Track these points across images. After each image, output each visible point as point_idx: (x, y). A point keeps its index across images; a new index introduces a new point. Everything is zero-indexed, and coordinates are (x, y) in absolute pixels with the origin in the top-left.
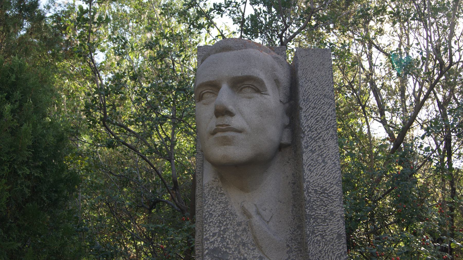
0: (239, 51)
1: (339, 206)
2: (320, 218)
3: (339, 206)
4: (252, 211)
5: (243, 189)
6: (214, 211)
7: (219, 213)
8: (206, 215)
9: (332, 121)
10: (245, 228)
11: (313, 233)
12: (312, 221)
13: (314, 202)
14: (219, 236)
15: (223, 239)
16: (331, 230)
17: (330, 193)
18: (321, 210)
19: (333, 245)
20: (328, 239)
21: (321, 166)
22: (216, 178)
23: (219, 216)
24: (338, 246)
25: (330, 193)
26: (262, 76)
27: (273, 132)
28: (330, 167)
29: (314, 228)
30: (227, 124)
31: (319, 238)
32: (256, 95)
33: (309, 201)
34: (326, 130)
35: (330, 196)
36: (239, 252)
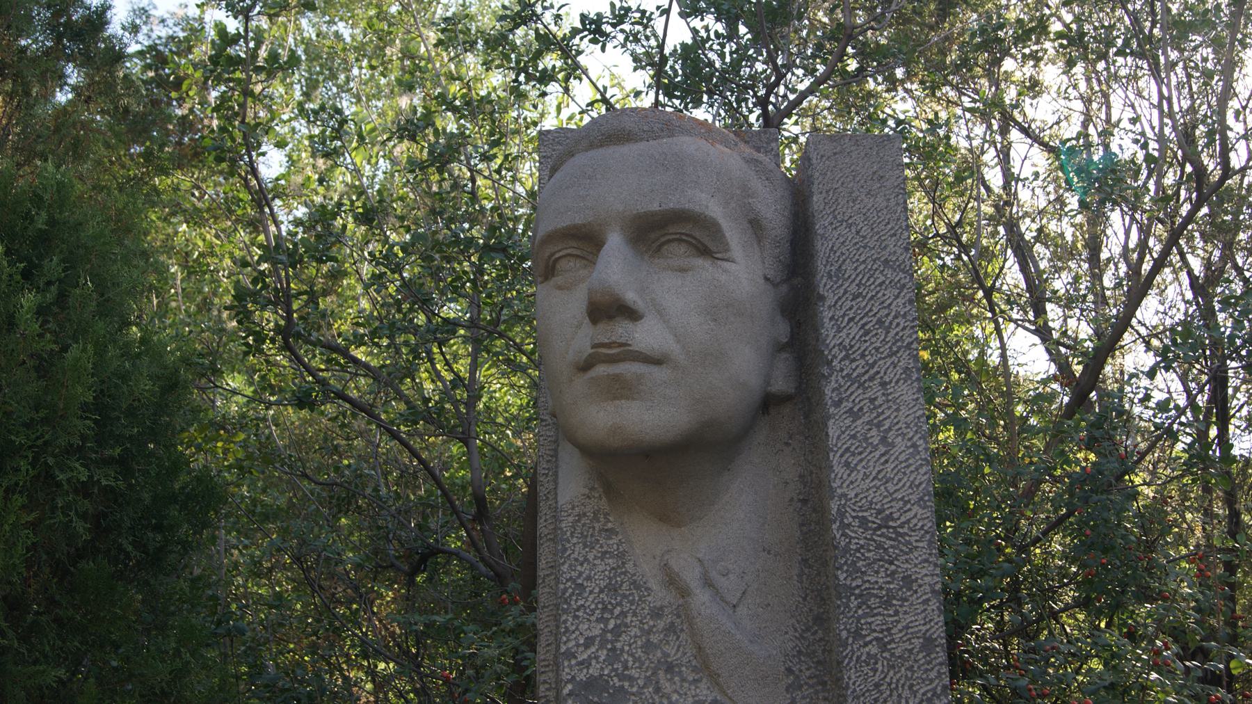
1: (926, 561)
3: (926, 561)
4: (692, 576)
5: (668, 517)
6: (589, 578)
7: (603, 584)
8: (566, 590)
9: (907, 332)
10: (672, 623)
11: (857, 634)
12: (854, 603)
13: (858, 550)
14: (601, 647)
15: (614, 655)
16: (907, 627)
17: (901, 526)
18: (877, 572)
19: (911, 668)
20: (898, 652)
21: (877, 454)
22: (592, 489)
23: (601, 591)
24: (926, 670)
25: (901, 526)
26: (715, 210)
28: (902, 457)
29: (858, 621)
30: (622, 340)
31: (874, 649)
32: (699, 261)
33: (846, 550)
34: (890, 356)
35: (903, 535)
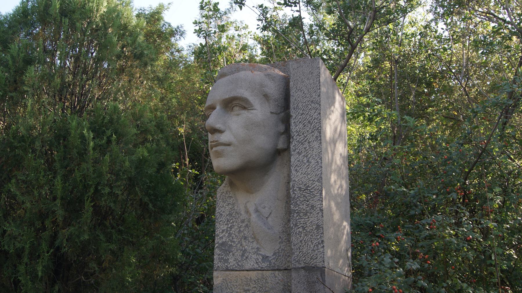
0: (232, 75)
1: (319, 200)
2: (302, 212)
3: (319, 200)
4: (252, 210)
5: (250, 191)
6: (224, 212)
7: (228, 213)
9: (317, 124)
10: (247, 224)
11: (296, 225)
12: (295, 215)
13: (297, 198)
16: (312, 222)
17: (312, 189)
18: (303, 205)
19: (312, 235)
20: (308, 230)
21: (306, 166)
24: (317, 236)
25: (312, 189)
26: (246, 94)
27: (263, 142)
28: (313, 166)
29: (296, 220)
30: (216, 140)
31: (301, 230)
32: (243, 111)
33: (294, 198)
34: (311, 133)
36: (241, 245)
